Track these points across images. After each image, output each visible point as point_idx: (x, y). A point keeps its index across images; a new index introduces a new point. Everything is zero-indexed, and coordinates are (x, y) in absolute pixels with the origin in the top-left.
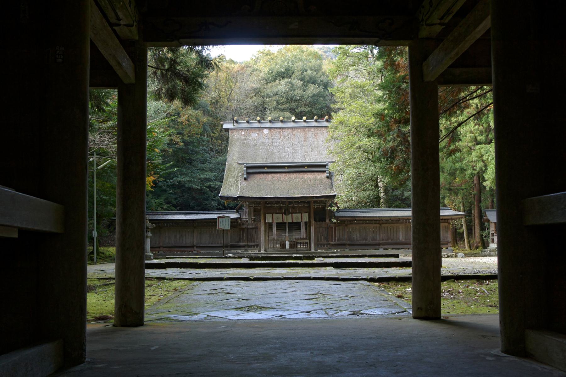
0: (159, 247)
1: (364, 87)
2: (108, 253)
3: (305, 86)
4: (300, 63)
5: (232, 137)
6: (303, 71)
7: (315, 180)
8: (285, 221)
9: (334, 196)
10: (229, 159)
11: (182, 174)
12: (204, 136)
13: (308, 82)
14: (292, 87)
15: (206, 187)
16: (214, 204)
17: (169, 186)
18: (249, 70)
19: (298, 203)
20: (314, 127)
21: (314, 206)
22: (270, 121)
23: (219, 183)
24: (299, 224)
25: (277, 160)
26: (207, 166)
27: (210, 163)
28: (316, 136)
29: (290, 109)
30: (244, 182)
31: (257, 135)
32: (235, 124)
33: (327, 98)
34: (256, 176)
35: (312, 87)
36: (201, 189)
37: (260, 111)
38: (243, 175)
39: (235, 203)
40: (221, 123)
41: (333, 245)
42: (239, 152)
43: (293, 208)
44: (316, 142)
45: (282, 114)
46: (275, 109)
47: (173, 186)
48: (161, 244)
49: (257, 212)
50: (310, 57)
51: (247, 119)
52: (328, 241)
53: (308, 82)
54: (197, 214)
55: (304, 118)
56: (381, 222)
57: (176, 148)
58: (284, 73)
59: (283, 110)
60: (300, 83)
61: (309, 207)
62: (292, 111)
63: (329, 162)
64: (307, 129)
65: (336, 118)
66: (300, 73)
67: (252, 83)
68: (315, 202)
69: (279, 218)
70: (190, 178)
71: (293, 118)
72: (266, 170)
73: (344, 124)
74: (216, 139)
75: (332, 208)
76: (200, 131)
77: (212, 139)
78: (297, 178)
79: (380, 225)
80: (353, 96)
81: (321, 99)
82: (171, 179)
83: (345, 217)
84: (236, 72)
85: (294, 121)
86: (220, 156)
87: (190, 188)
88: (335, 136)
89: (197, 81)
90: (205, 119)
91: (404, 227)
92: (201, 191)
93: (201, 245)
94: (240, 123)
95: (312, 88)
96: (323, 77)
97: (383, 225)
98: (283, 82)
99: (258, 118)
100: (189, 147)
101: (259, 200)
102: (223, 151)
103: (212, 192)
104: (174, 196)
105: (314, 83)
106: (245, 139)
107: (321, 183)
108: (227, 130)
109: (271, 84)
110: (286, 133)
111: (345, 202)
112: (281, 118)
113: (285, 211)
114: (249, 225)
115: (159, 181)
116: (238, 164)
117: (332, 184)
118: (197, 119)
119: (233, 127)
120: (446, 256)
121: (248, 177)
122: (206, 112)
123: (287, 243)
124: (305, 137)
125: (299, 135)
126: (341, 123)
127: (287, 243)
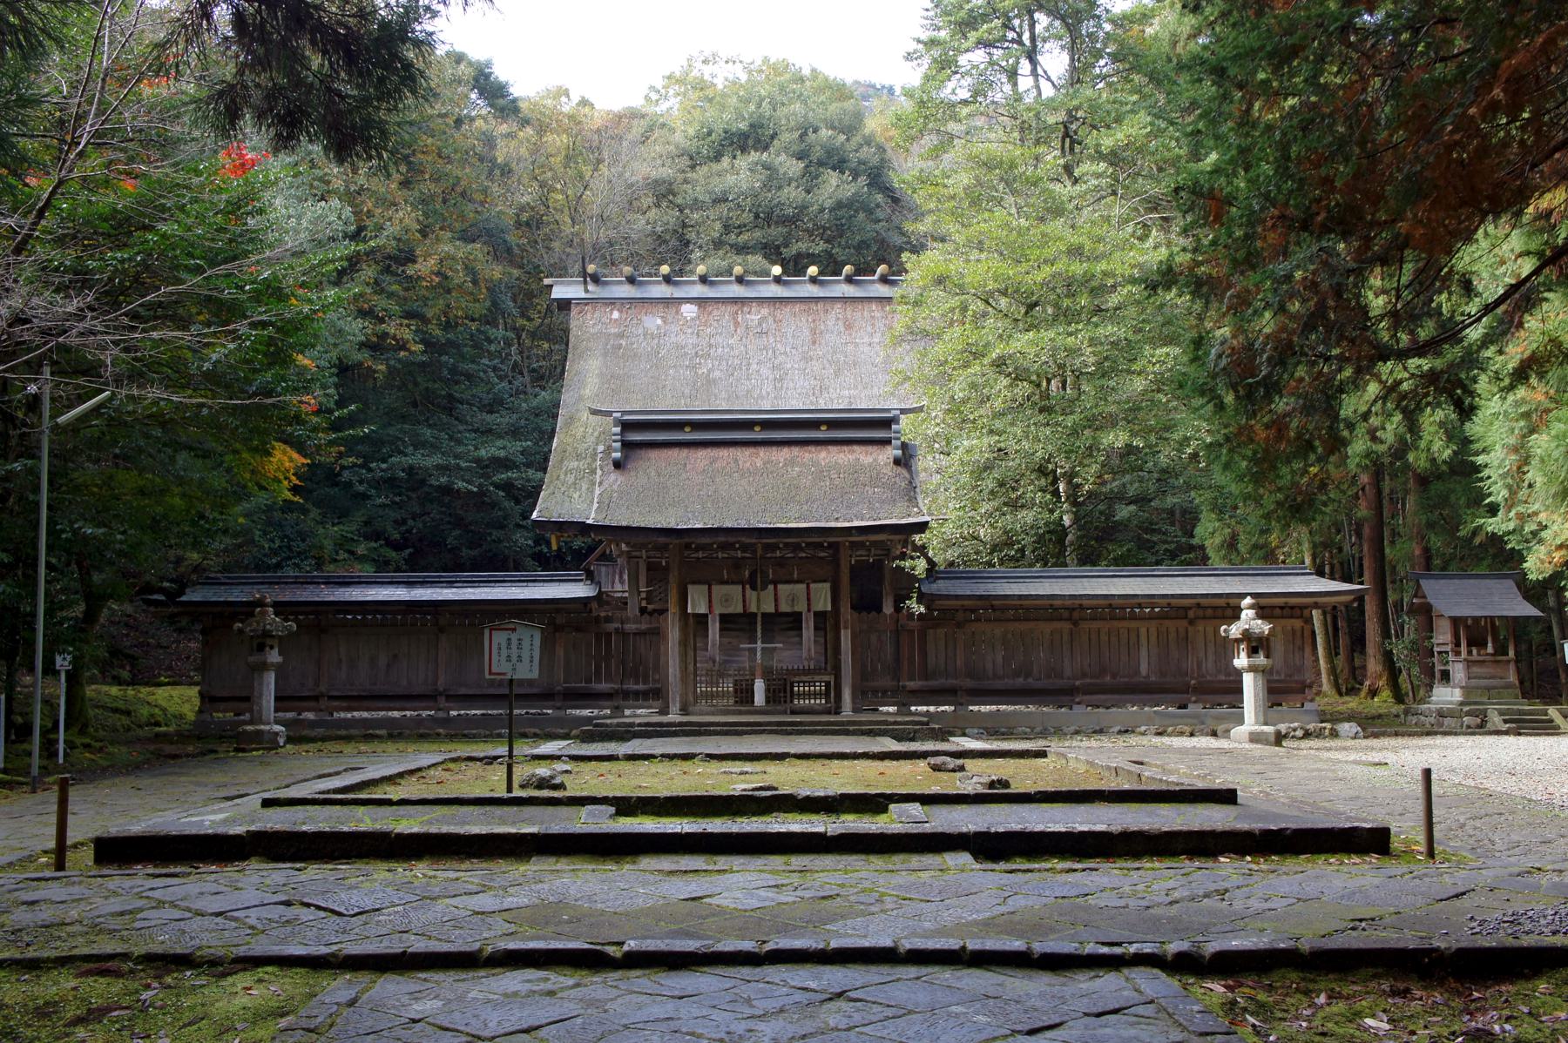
0: (316, 698)
1: (1013, 166)
2: (145, 711)
3: (810, 179)
4: (797, 107)
5: (580, 327)
6: (805, 130)
7: (856, 469)
8: (753, 609)
9: (922, 527)
10: (567, 397)
11: (419, 444)
12: (497, 327)
13: (821, 163)
14: (770, 178)
15: (497, 486)
16: (523, 540)
17: (377, 484)
18: (638, 128)
19: (796, 547)
20: (844, 299)
21: (848, 560)
22: (704, 280)
23: (539, 475)
24: (794, 621)
25: (723, 401)
26: (502, 420)
27: (512, 410)
28: (848, 327)
29: (765, 246)
30: (613, 477)
31: (659, 321)
32: (590, 288)
33: (880, 214)
34: (654, 454)
35: (832, 179)
36: (482, 493)
37: (674, 249)
38: (609, 449)
39: (577, 547)
40: (547, 281)
41: (913, 692)
42: (601, 375)
43: (781, 563)
44: (850, 347)
45: (739, 259)
46: (718, 244)
47: (391, 483)
48: (323, 688)
49: (656, 573)
50: (822, 98)
51: (627, 270)
52: (896, 678)
53: (821, 163)
54: (451, 584)
55: (813, 270)
56: (1076, 615)
57: (399, 360)
58: (744, 136)
59: (742, 250)
60: (795, 167)
61: (835, 562)
62: (772, 252)
63: (903, 411)
64: (820, 305)
65: (919, 269)
66: (796, 135)
67: (646, 167)
68: (854, 545)
69: (731, 598)
70: (446, 457)
71: (777, 270)
72: (757, 434)
73: (949, 285)
74: (533, 335)
75: (907, 564)
76: (479, 309)
77: (519, 338)
78: (791, 462)
79: (1075, 624)
80: (976, 199)
81: (861, 216)
82: (384, 461)
83: (957, 597)
84: (598, 131)
85: (778, 280)
86: (544, 388)
87: (447, 490)
88: (921, 324)
89: (395, 56)
90: (496, 272)
91: (1153, 630)
92: (480, 500)
93: (463, 691)
94: (606, 283)
95: (834, 182)
96: (865, 148)
97: (1085, 625)
98: (743, 162)
99: (665, 269)
100: (444, 358)
101: (662, 540)
102: (552, 374)
103: (517, 502)
104: (393, 514)
105: (840, 165)
106: (621, 335)
107: (875, 480)
108: (565, 304)
109: (705, 168)
110: (754, 316)
111: (950, 544)
112: (738, 270)
113: (753, 574)
114: (628, 620)
115: (343, 467)
116: (595, 412)
117: (912, 487)
118: (470, 270)
119: (583, 295)
120: (1299, 733)
121: (626, 457)
122: (502, 251)
123: (759, 687)
124: (813, 332)
125: (795, 324)
126: (940, 281)
127: (759, 687)
